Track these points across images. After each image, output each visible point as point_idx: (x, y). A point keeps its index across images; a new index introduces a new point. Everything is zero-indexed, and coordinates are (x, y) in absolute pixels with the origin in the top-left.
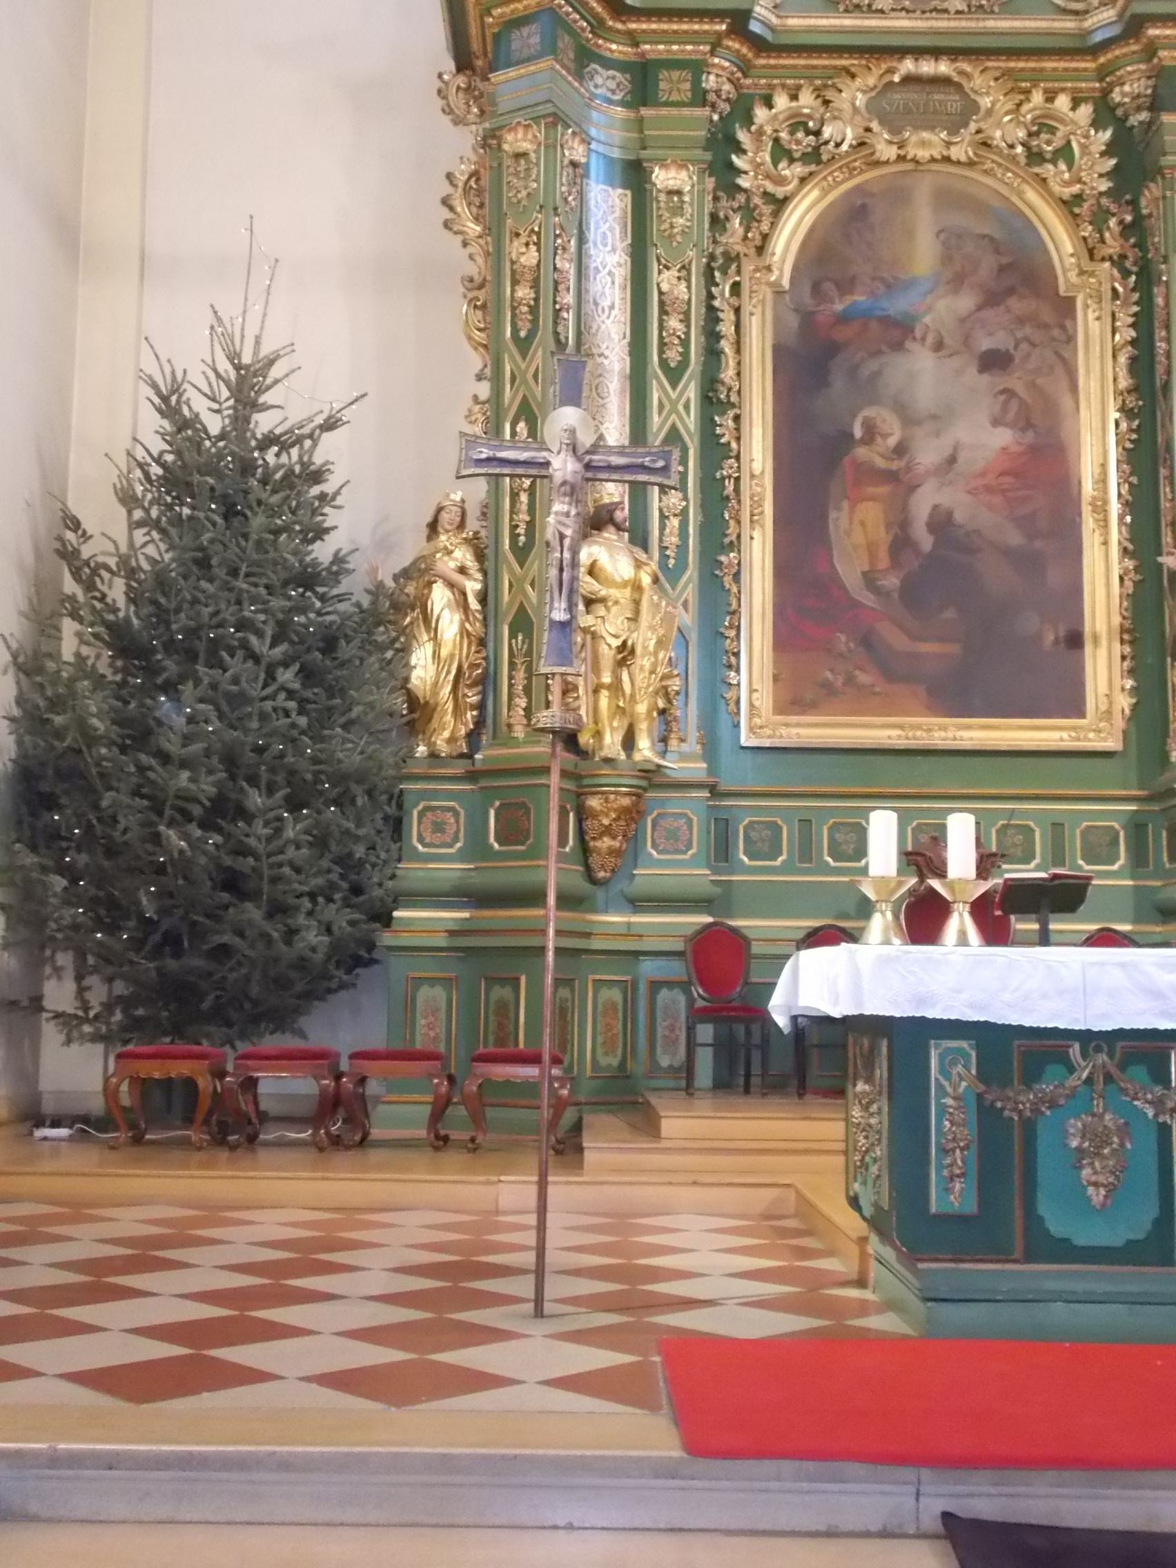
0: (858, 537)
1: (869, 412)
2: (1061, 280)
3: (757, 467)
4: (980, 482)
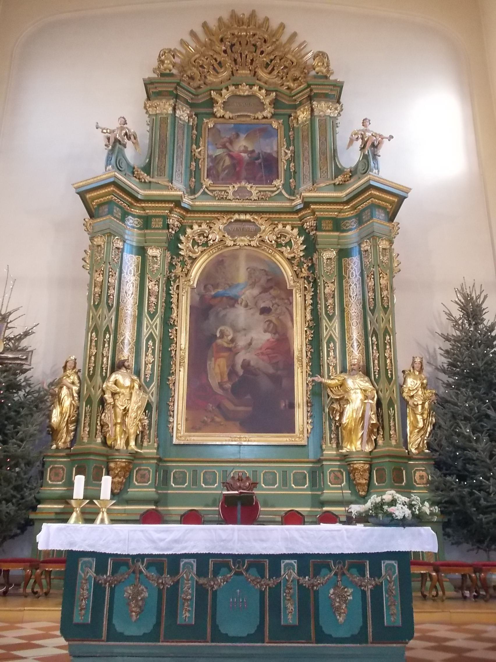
0: (217, 370)
1: (222, 328)
2: (288, 284)
3: (183, 346)
4: (259, 351)
